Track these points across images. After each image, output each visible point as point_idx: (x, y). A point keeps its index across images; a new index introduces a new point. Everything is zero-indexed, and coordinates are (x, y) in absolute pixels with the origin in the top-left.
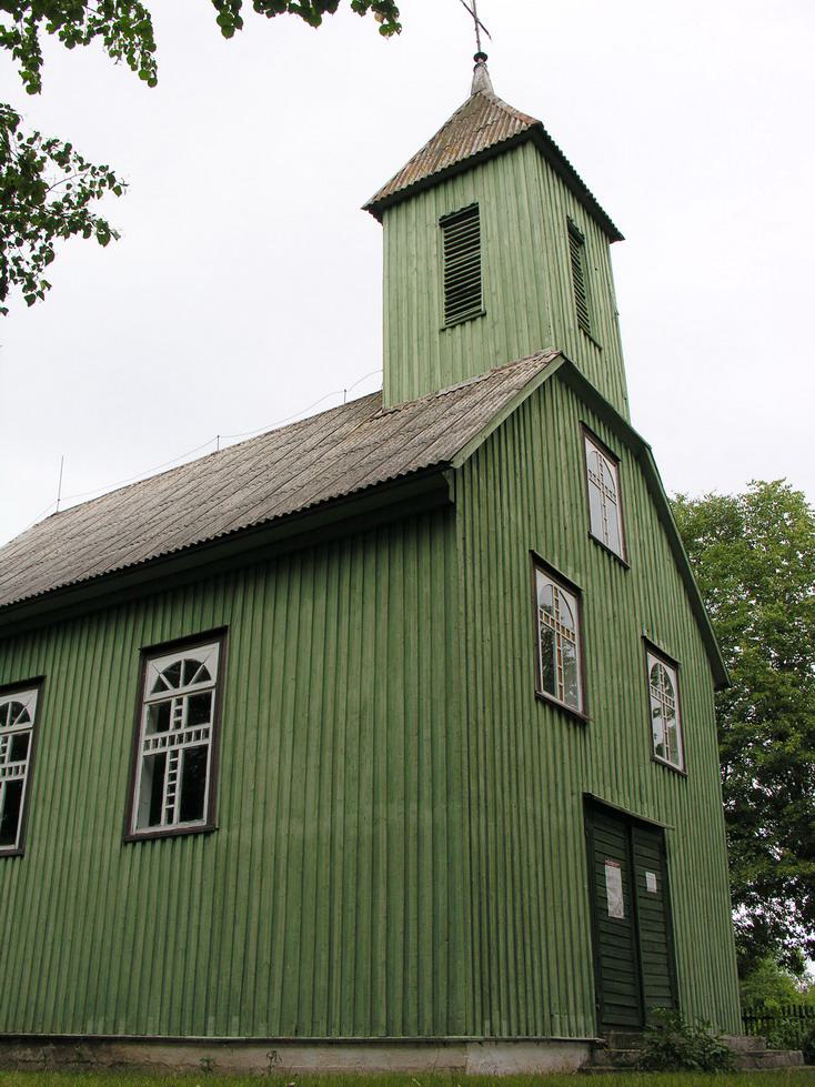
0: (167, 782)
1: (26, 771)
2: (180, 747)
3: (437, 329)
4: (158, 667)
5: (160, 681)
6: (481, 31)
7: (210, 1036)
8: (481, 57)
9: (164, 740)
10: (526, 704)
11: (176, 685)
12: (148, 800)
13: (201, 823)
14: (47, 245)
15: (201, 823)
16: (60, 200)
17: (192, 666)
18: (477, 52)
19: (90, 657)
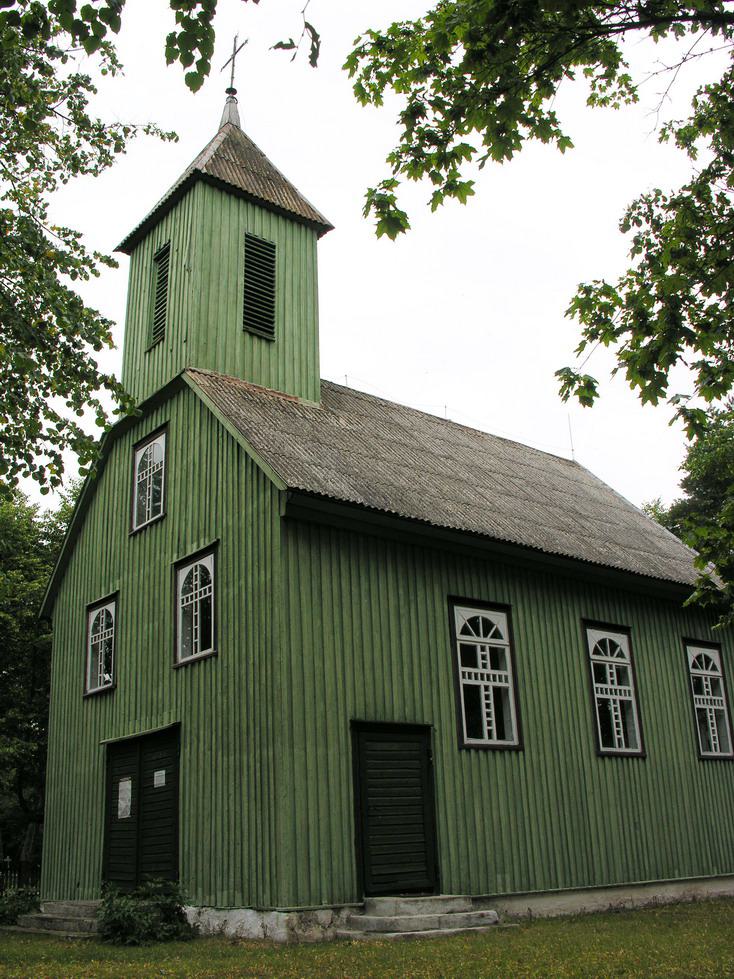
0: (491, 701)
1: (461, 674)
2: (491, 684)
3: (144, 351)
4: (463, 615)
5: (465, 627)
6: (231, 62)
7: (560, 889)
8: (231, 91)
9: (187, 598)
10: (125, 591)
11: (485, 635)
12: (506, 719)
13: (210, 651)
14: (444, 173)
15: (210, 651)
16: (608, 88)
17: (488, 625)
18: (229, 87)
19: (148, 539)
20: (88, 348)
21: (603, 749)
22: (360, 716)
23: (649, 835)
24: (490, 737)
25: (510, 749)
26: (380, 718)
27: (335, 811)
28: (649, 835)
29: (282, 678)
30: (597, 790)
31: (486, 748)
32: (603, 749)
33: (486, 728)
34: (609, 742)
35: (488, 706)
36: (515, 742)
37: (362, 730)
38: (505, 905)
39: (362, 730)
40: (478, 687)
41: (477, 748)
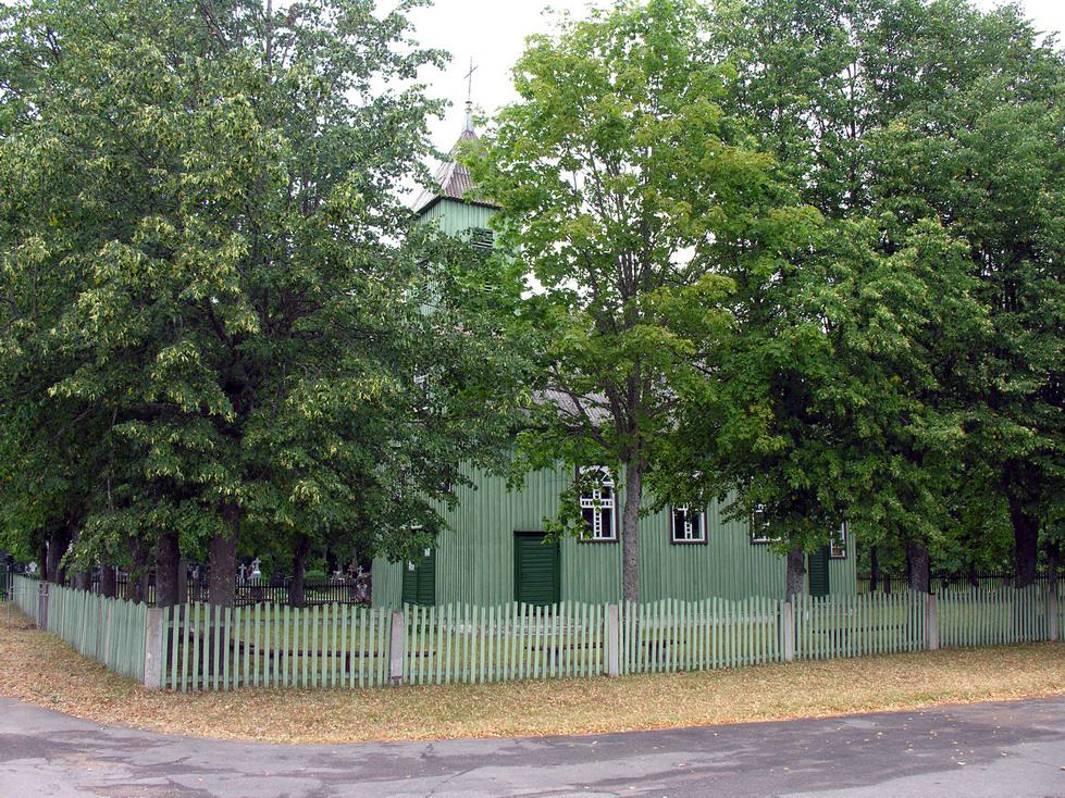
20: (248, 13)
21: (675, 540)
22: (520, 529)
23: (704, 588)
24: (689, 537)
25: (701, 543)
26: (535, 530)
27: (504, 576)
28: (704, 588)
29: (477, 512)
30: (668, 564)
31: (685, 543)
32: (675, 540)
33: (686, 532)
34: (680, 534)
35: (598, 519)
36: (703, 540)
37: (518, 534)
38: (834, 731)
39: (518, 534)
40: (592, 509)
41: (680, 543)
